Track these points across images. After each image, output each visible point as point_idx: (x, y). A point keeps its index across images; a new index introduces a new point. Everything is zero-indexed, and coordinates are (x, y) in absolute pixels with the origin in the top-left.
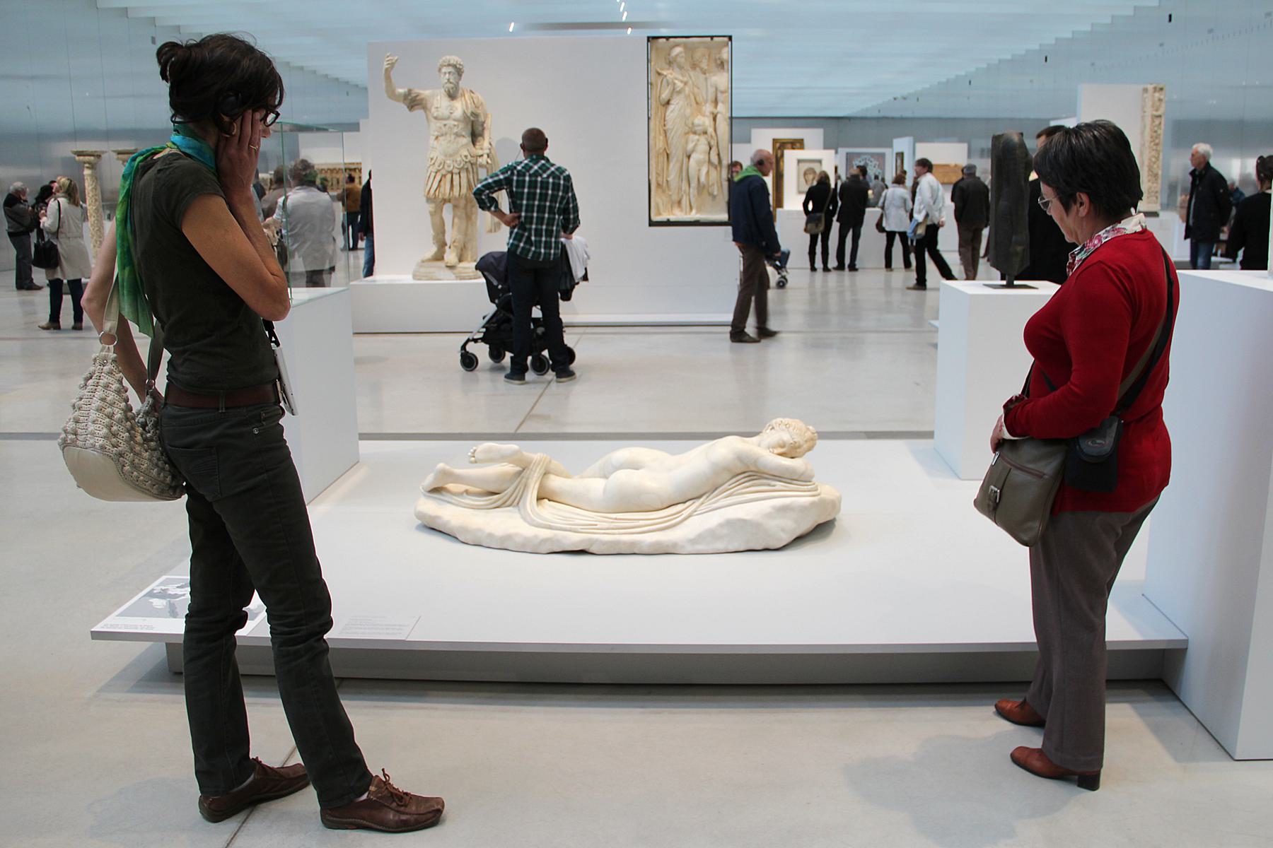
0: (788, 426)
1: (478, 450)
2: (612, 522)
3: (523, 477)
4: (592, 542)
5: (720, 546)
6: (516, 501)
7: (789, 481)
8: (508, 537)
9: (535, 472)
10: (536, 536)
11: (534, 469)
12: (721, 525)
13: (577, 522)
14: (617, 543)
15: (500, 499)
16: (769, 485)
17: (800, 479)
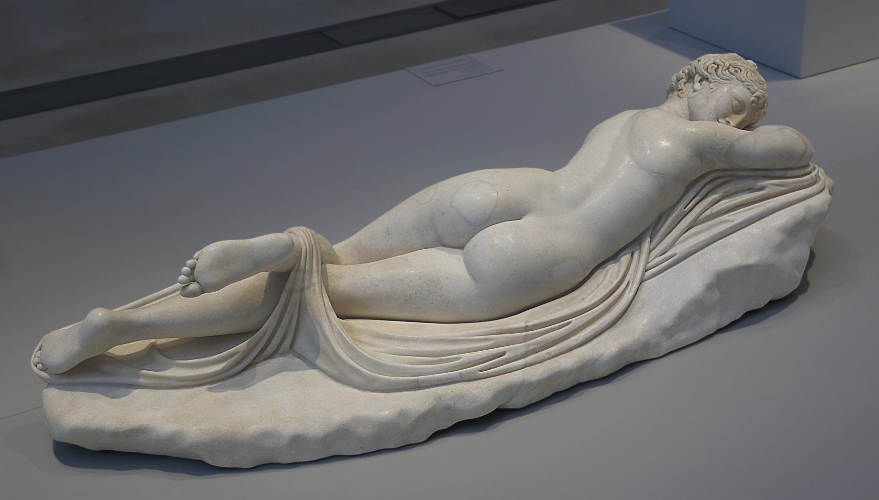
0: (732, 69)
2: (526, 339)
3: (291, 292)
4: (511, 390)
5: (712, 324)
6: (288, 342)
8: (343, 432)
9: (311, 272)
10: (403, 414)
11: (307, 268)
12: (709, 287)
13: (466, 357)
14: (558, 375)
15: (256, 345)
16: (752, 190)
17: (797, 166)
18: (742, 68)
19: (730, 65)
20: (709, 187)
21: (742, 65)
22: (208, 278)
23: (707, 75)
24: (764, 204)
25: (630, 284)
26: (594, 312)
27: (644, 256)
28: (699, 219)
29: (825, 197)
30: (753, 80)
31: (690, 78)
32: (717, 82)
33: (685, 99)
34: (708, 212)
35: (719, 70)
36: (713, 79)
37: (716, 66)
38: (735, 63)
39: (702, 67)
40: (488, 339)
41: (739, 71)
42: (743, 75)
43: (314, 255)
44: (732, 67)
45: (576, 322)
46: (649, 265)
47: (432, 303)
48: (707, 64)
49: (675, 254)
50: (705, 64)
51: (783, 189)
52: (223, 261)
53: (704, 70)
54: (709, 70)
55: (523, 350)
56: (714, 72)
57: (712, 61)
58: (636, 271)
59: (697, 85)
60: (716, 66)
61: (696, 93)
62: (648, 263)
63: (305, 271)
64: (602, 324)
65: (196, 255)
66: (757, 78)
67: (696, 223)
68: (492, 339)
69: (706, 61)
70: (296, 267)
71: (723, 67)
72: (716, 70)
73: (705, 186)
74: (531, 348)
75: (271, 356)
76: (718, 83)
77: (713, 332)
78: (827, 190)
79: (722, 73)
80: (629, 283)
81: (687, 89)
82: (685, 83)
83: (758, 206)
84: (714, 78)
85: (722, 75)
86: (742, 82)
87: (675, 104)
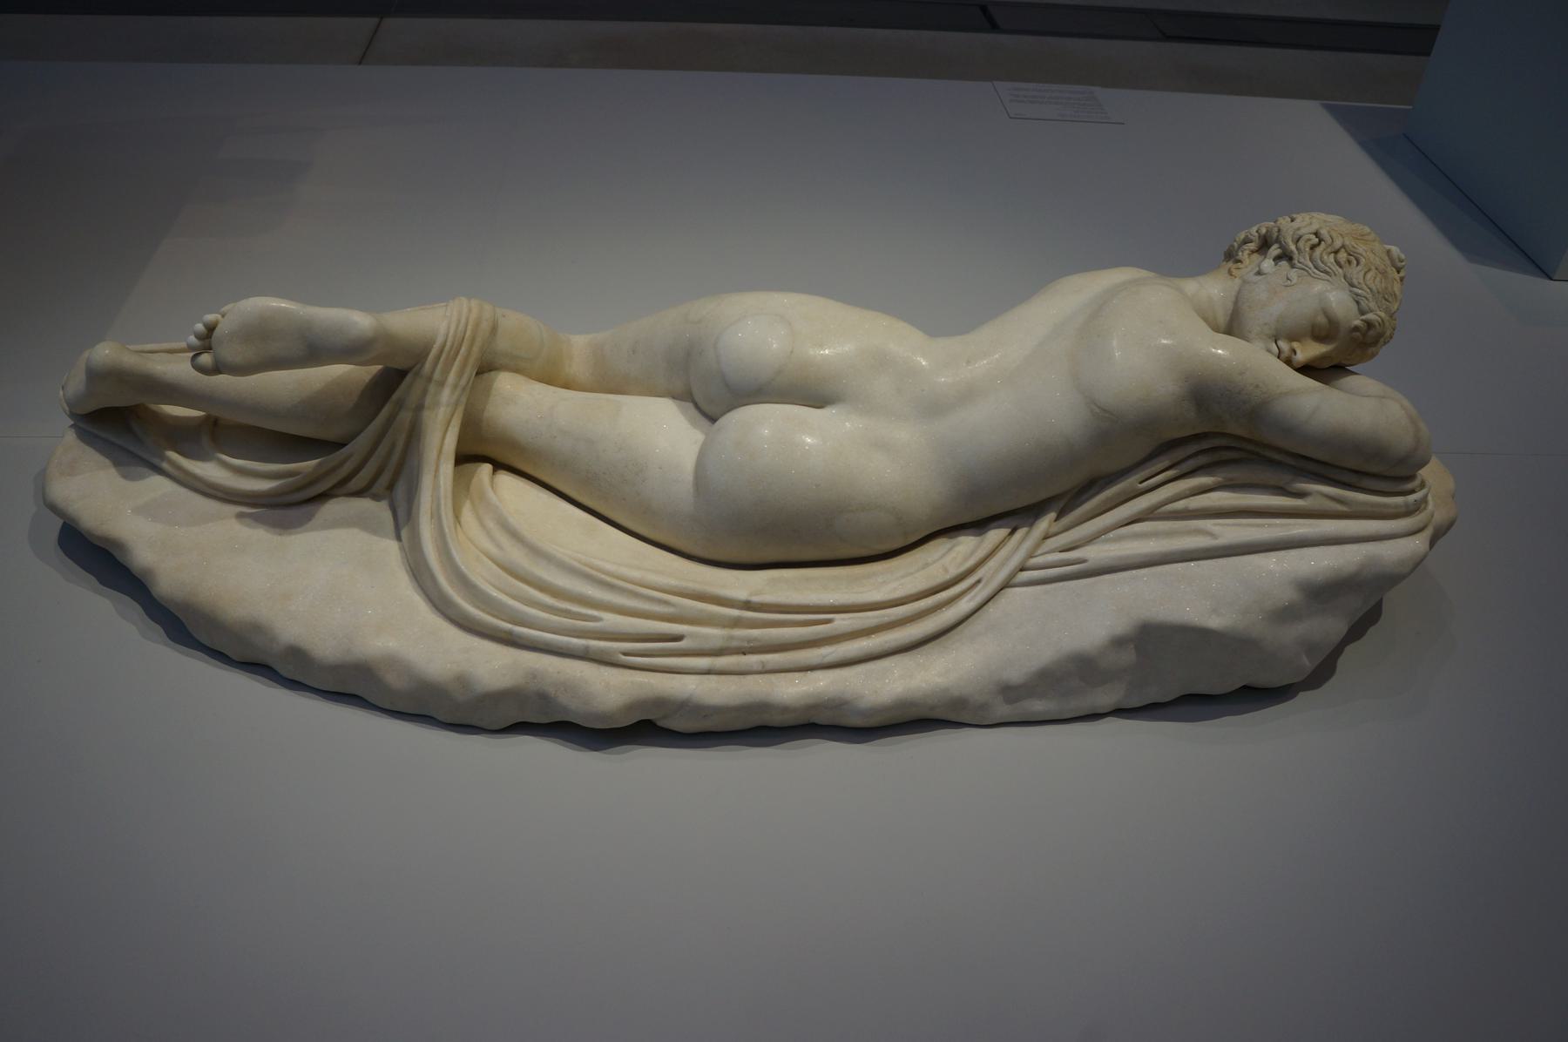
0: (1342, 256)
1: (223, 329)
2: (737, 623)
3: (400, 405)
5: (1105, 698)
6: (384, 480)
7: (1352, 479)
9: (442, 384)
11: (437, 376)
12: (1118, 642)
13: (611, 620)
14: (763, 706)
15: (333, 470)
18: (1363, 261)
19: (1343, 246)
20: (1202, 460)
21: (1364, 254)
22: (231, 352)
23: (1292, 252)
24: (1290, 524)
25: (980, 586)
26: (884, 616)
27: (1028, 544)
28: (1163, 509)
29: (1418, 544)
30: (1374, 288)
31: (1264, 245)
32: (1307, 271)
33: (1238, 281)
34: (1180, 505)
35: (1318, 251)
36: (1300, 263)
37: (1317, 240)
38: (1354, 247)
39: (1291, 233)
40: (666, 603)
41: (1355, 262)
42: (1358, 273)
43: (459, 358)
44: (1346, 251)
45: (842, 622)
46: (1033, 561)
47: (624, 499)
48: (1300, 233)
49: (1084, 561)
50: (1299, 229)
51: (1340, 507)
52: (259, 331)
53: (1292, 241)
54: (1301, 244)
55: (719, 644)
56: (1308, 249)
57: (1314, 227)
58: (1003, 564)
59: (1268, 264)
60: (1317, 240)
61: (1259, 278)
62: (1032, 557)
63: (430, 379)
64: (886, 642)
65: (224, 309)
66: (1383, 285)
67: (1151, 516)
68: (672, 605)
69: (1305, 223)
70: (418, 366)
71: (1327, 247)
72: (1313, 247)
73: (1190, 457)
74: (735, 644)
75: (359, 493)
76: (1306, 273)
77: (1105, 711)
78: (1428, 533)
79: (1321, 258)
80: (979, 581)
81: (1249, 261)
82: (1253, 252)
83: (1276, 525)
84: (1302, 260)
85: (1319, 261)
86: (1352, 285)
87: (1214, 289)
